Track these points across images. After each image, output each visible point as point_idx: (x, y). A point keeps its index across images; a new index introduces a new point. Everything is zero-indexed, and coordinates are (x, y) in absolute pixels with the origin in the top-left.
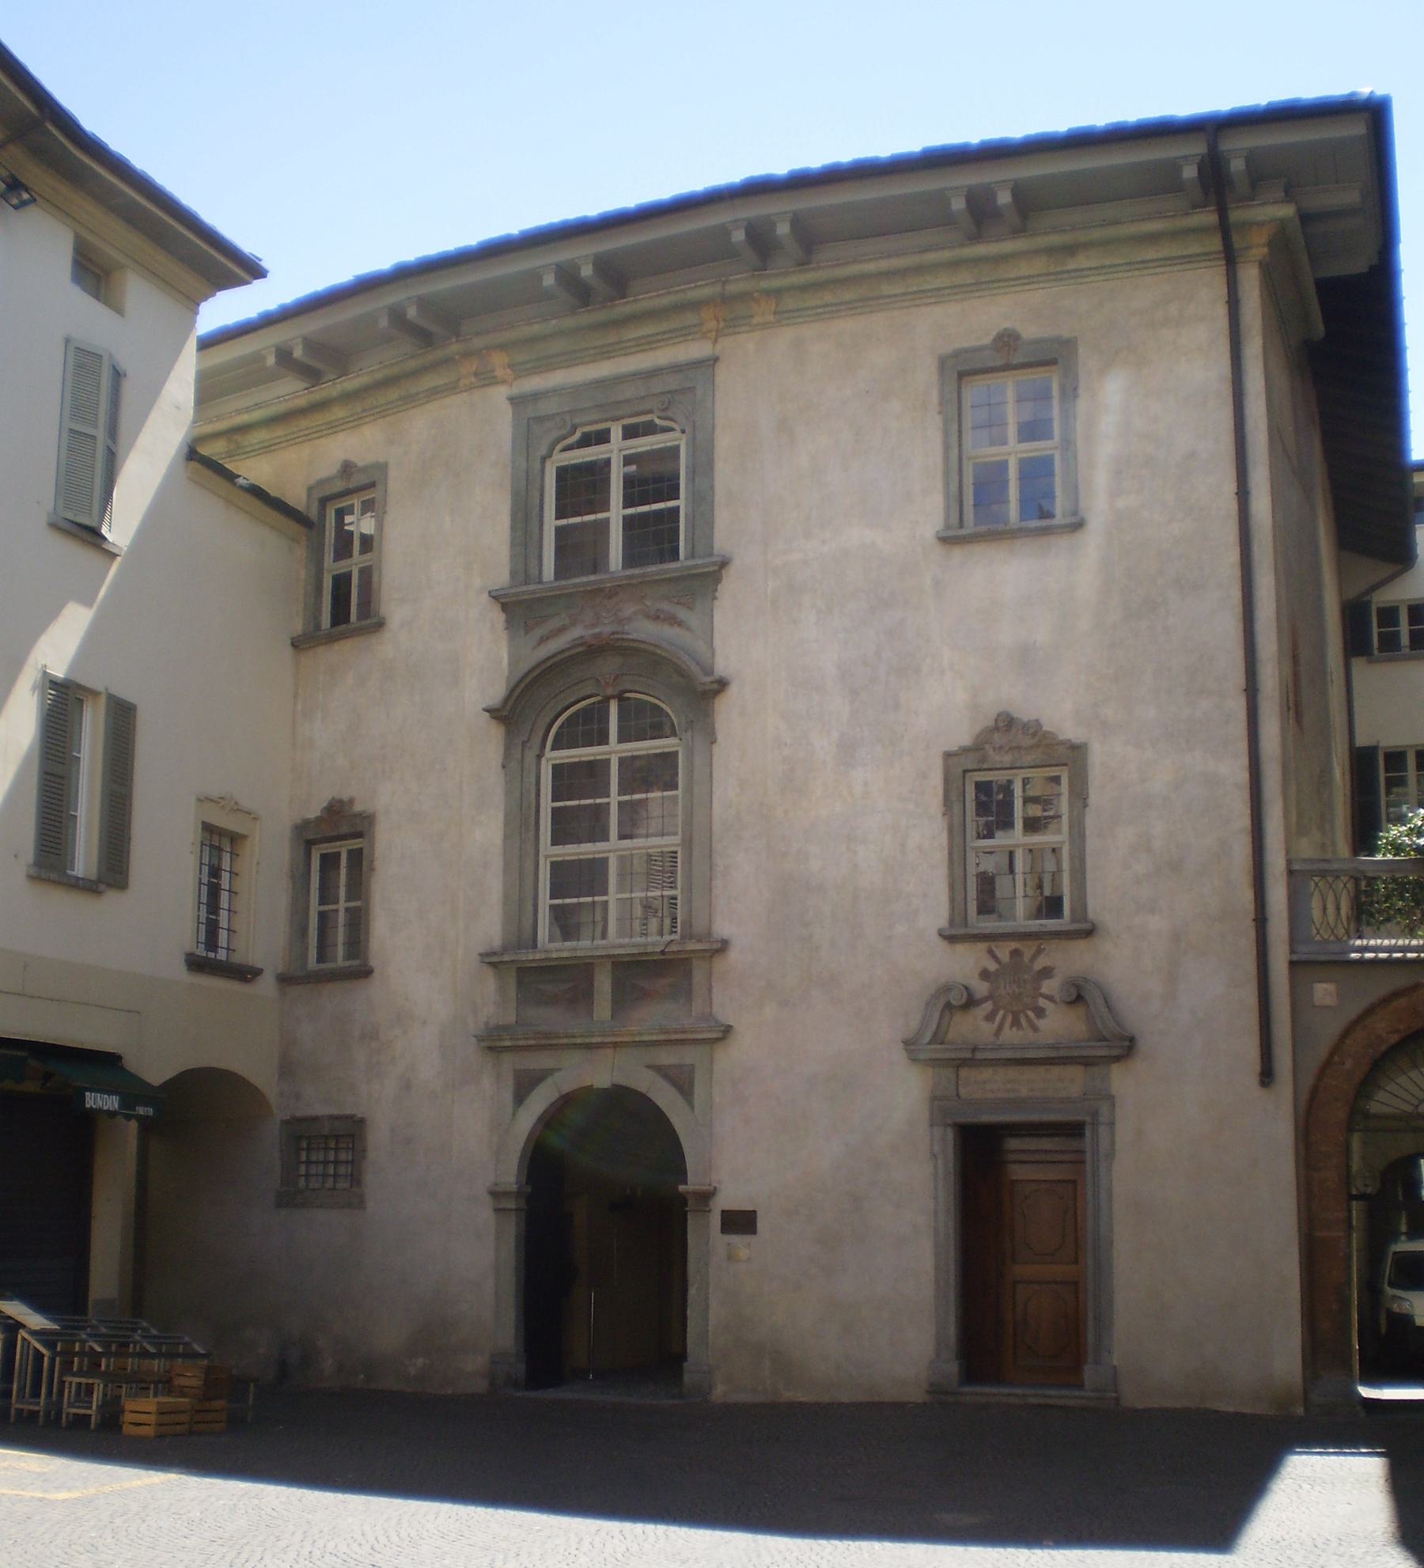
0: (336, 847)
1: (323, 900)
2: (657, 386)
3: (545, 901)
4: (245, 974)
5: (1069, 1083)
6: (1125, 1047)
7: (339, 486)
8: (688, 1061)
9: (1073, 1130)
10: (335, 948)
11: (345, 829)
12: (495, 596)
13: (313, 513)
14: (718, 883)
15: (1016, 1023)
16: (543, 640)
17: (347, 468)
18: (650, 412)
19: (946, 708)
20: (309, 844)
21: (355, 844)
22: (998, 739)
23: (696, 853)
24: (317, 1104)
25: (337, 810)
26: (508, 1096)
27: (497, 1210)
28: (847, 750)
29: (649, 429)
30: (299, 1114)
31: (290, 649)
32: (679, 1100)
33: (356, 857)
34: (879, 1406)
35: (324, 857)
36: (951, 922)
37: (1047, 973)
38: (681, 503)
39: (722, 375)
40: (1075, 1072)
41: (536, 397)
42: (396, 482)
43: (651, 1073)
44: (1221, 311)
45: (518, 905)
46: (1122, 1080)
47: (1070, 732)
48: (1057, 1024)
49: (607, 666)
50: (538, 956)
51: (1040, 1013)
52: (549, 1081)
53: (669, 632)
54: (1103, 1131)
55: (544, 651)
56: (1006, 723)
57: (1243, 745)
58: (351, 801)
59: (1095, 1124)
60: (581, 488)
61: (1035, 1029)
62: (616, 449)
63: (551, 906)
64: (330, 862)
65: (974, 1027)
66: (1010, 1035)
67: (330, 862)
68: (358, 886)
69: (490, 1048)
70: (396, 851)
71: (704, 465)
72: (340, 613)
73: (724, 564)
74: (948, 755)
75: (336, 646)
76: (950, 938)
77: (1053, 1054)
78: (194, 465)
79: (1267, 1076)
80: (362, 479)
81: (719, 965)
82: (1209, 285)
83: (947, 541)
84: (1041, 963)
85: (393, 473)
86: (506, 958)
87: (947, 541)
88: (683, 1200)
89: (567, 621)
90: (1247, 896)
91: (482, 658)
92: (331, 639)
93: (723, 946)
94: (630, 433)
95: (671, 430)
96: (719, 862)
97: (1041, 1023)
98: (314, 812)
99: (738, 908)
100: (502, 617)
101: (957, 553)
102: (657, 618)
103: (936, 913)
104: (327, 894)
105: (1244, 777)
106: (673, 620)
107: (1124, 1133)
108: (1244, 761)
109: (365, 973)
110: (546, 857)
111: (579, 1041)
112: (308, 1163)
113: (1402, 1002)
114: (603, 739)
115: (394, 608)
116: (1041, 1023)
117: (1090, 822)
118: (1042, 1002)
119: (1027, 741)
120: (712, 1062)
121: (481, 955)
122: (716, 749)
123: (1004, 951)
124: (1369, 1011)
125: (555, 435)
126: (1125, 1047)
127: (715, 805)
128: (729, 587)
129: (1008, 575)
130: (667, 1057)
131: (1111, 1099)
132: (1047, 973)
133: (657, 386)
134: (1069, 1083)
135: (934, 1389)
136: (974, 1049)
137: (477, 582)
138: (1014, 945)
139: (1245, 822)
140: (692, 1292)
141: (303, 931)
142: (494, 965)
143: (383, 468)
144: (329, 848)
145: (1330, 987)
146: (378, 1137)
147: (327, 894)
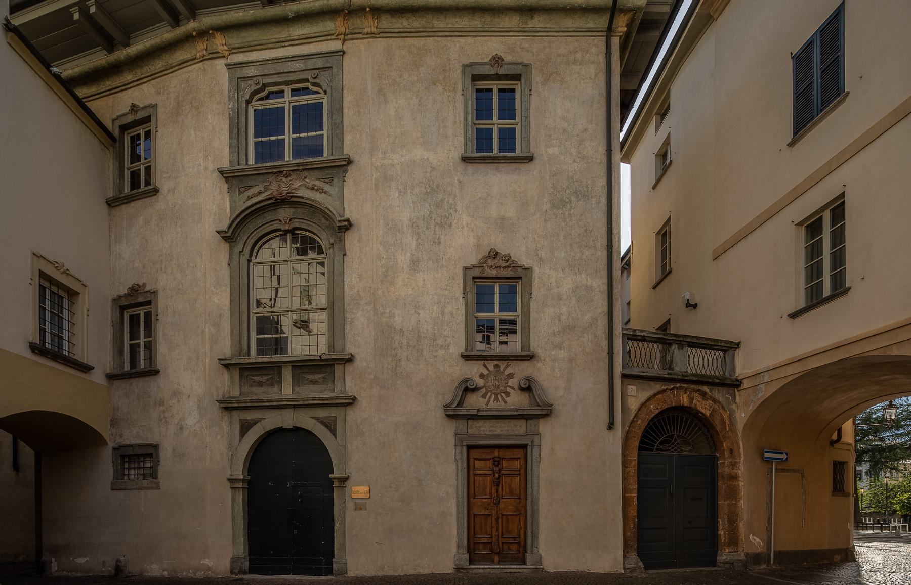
0: (136, 312)
1: (132, 338)
2: (311, 64)
3: (254, 336)
4: (85, 368)
5: (520, 428)
6: (546, 412)
7: (130, 119)
8: (333, 415)
9: (524, 447)
10: (137, 364)
11: (141, 300)
12: (221, 172)
13: (116, 133)
14: (348, 327)
15: (496, 399)
16: (249, 198)
17: (134, 108)
18: (307, 80)
19: (463, 244)
20: (123, 308)
21: (146, 309)
22: (490, 262)
23: (336, 311)
24: (131, 436)
25: (135, 290)
26: (237, 432)
27: (232, 488)
28: (415, 264)
29: (306, 91)
30: (123, 443)
31: (105, 207)
32: (329, 434)
33: (148, 316)
34: (249, 526)
35: (131, 317)
36: (466, 350)
37: (511, 376)
38: (325, 132)
39: (347, 60)
40: (522, 423)
41: (242, 64)
42: (162, 114)
43: (314, 421)
44: (602, 59)
45: (239, 337)
46: (544, 427)
47: (525, 262)
48: (516, 400)
49: (285, 213)
50: (251, 361)
51: (508, 394)
52: (259, 424)
53: (318, 197)
54: (536, 449)
55: (249, 203)
56: (494, 255)
57: (605, 273)
58: (144, 285)
59: (532, 446)
60: (269, 122)
61: (505, 402)
62: (287, 102)
63: (255, 143)
64: (134, 320)
65: (475, 402)
66: (493, 404)
67: (134, 320)
68: (149, 331)
69: (226, 408)
70: (168, 309)
71: (338, 109)
72: (135, 184)
73: (350, 162)
74: (466, 269)
75: (132, 204)
76: (466, 358)
77: (516, 413)
78: (10, 34)
79: (611, 426)
80: (141, 115)
81: (349, 368)
82: (596, 46)
83: (465, 160)
84: (509, 371)
85: (160, 110)
86: (233, 362)
87: (465, 160)
88: (331, 481)
89: (262, 189)
90: (605, 343)
91: (215, 205)
92: (129, 199)
93: (350, 360)
94: (295, 92)
95: (318, 93)
96: (349, 316)
97: (508, 399)
98: (123, 291)
99: (360, 338)
100: (226, 186)
101: (471, 168)
102: (313, 189)
103: (458, 346)
104: (134, 335)
105: (605, 288)
106: (322, 191)
107: (545, 450)
108: (605, 280)
109: (154, 372)
110: (254, 313)
111: (275, 404)
112: (129, 469)
113: (660, 396)
114: (296, 110)
115: (162, 181)
116: (508, 399)
117: (533, 306)
118: (508, 389)
119: (504, 264)
120: (346, 415)
121: (219, 360)
122: (346, 259)
123: (491, 365)
124: (649, 399)
125: (254, 88)
126: (546, 412)
127: (346, 287)
128: (352, 173)
129: (498, 182)
130: (322, 413)
131: (539, 434)
132: (511, 376)
133: (311, 64)
134: (515, 431)
135: (458, 569)
136: (478, 410)
137: (211, 167)
138: (496, 362)
139: (605, 309)
140: (337, 525)
141: (121, 352)
142: (227, 366)
143: (154, 106)
144: (134, 312)
145: (634, 387)
146: (165, 455)
147: (134, 335)
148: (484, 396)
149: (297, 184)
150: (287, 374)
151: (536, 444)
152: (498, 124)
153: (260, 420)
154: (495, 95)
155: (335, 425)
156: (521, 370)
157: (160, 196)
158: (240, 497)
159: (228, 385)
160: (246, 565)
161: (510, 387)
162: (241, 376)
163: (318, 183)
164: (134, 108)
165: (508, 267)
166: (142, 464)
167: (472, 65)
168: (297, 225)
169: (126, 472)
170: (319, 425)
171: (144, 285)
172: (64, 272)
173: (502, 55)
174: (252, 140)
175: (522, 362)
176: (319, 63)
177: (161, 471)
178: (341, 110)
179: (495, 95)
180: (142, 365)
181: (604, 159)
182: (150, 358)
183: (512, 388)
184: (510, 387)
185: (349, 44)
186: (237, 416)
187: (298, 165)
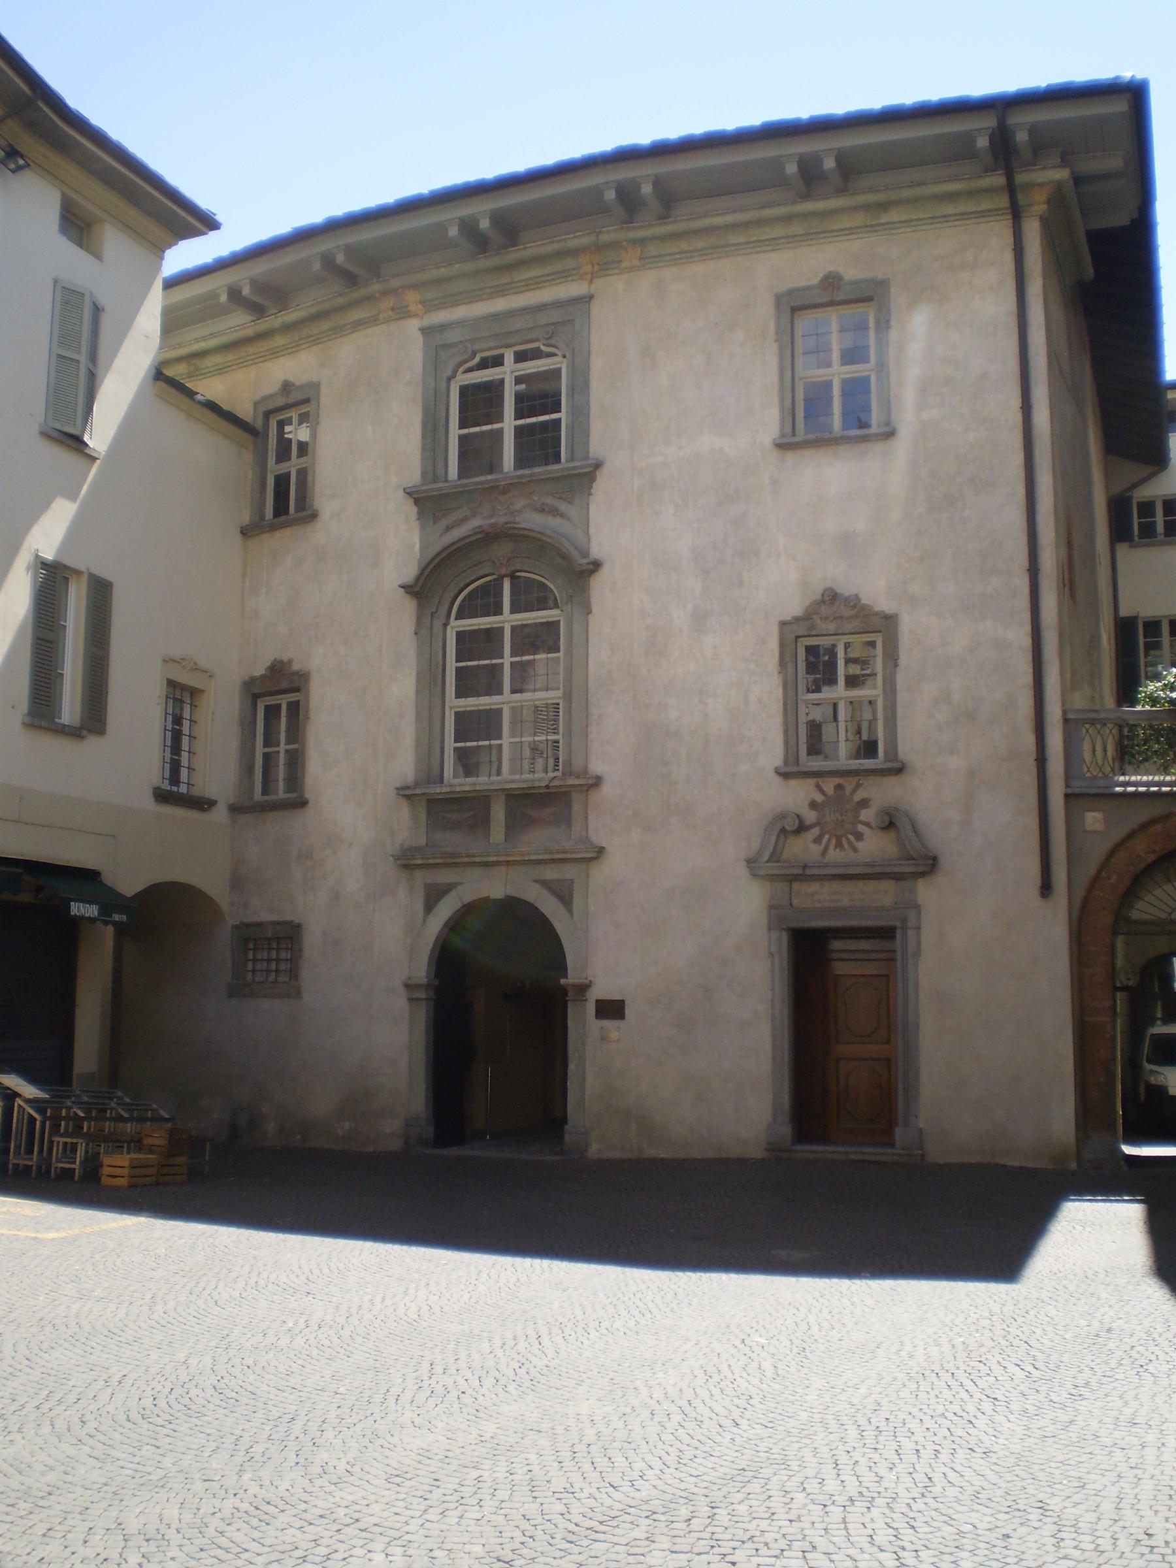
0: (277, 699)
2: (543, 319)
4: (202, 804)
5: (883, 894)
6: (929, 865)
7: (280, 401)
8: (568, 876)
9: (886, 933)
10: (276, 783)
11: (284, 685)
12: (409, 493)
13: (259, 424)
14: (593, 729)
15: (839, 845)
16: (449, 528)
17: (287, 387)
18: (537, 340)
19: (781, 585)
22: (824, 610)
24: (261, 912)
25: (278, 669)
26: (419, 905)
28: (700, 619)
30: (246, 920)
31: (238, 537)
32: (561, 908)
33: (294, 708)
35: (267, 708)
36: (786, 762)
37: (864, 803)
38: (562, 415)
40: (888, 885)
41: (442, 328)
42: (327, 398)
44: (1009, 257)
45: (428, 749)
46: (926, 892)
47: (884, 604)
48: (873, 846)
50: (444, 790)
51: (859, 836)
52: (453, 893)
53: (552, 522)
54: (911, 934)
55: (449, 538)
56: (831, 597)
57: (1026, 616)
58: (290, 662)
59: (904, 929)
60: (480, 403)
61: (855, 850)
62: (508, 371)
64: (272, 712)
66: (834, 855)
67: (272, 712)
68: (296, 732)
69: (405, 866)
70: (326, 703)
71: (581, 384)
72: (281, 506)
73: (598, 466)
74: (783, 624)
75: (278, 534)
76: (785, 775)
79: (1046, 888)
80: (299, 396)
81: (594, 797)
82: (998, 235)
83: (782, 446)
85: (324, 391)
86: (418, 791)
88: (564, 991)
90: (1030, 740)
91: (398, 544)
92: (273, 528)
93: (597, 782)
94: (520, 357)
95: (554, 355)
96: (594, 711)
97: (860, 845)
98: (259, 671)
99: (610, 750)
100: (415, 509)
101: (791, 457)
102: (542, 511)
103: (773, 754)
104: (270, 739)
105: (1027, 641)
106: (556, 512)
107: (928, 935)
108: (1028, 628)
109: (302, 803)
110: (451, 708)
111: (478, 860)
112: (255, 960)
113: (1159, 827)
115: (325, 502)
116: (860, 845)
117: (901, 679)
118: (860, 828)
119: (849, 612)
122: (591, 618)
123: (829, 785)
124: (1131, 835)
125: (458, 359)
126: (929, 865)
127: (590, 664)
128: (602, 484)
130: (551, 873)
131: (917, 908)
132: (864, 803)
133: (543, 319)
134: (883, 894)
135: (772, 1148)
136: (805, 867)
138: (837, 781)
139: (1028, 679)
140: (572, 1067)
141: (251, 769)
143: (316, 386)
144: (272, 700)
145: (1099, 815)
146: (313, 939)
147: (270, 739)
148: (818, 840)
149: (519, 503)
150: (498, 813)
151: (911, 923)
152: (839, 374)
153: (454, 885)
154: (552, 737)
155: (571, 894)
156: (882, 793)
157: (319, 524)
158: (422, 1015)
159: (405, 827)
160: (430, 1131)
161: (864, 824)
162: (429, 813)
163: (549, 501)
164: (287, 387)
165: (857, 616)
166: (274, 955)
167: (791, 292)
168: (518, 567)
169: (250, 966)
170: (546, 895)
171: (290, 662)
172: (90, 371)
173: (841, 270)
174: (455, 432)
175: (884, 779)
176: (556, 316)
177: (306, 974)
178: (586, 385)
179: (552, 737)
180: (281, 792)
181: (1018, 418)
182: (295, 777)
183: (867, 824)
184: (864, 824)
185: (599, 283)
186: (420, 878)
187: (519, 477)
